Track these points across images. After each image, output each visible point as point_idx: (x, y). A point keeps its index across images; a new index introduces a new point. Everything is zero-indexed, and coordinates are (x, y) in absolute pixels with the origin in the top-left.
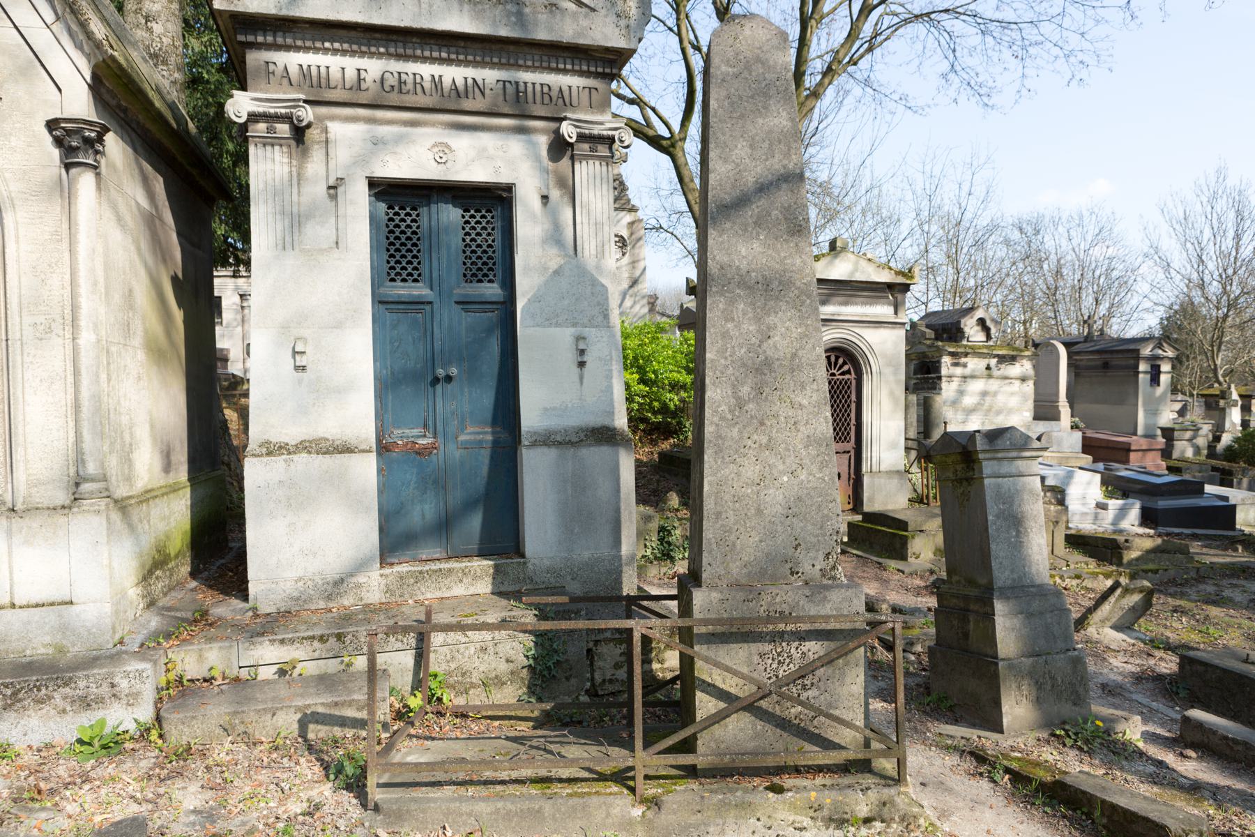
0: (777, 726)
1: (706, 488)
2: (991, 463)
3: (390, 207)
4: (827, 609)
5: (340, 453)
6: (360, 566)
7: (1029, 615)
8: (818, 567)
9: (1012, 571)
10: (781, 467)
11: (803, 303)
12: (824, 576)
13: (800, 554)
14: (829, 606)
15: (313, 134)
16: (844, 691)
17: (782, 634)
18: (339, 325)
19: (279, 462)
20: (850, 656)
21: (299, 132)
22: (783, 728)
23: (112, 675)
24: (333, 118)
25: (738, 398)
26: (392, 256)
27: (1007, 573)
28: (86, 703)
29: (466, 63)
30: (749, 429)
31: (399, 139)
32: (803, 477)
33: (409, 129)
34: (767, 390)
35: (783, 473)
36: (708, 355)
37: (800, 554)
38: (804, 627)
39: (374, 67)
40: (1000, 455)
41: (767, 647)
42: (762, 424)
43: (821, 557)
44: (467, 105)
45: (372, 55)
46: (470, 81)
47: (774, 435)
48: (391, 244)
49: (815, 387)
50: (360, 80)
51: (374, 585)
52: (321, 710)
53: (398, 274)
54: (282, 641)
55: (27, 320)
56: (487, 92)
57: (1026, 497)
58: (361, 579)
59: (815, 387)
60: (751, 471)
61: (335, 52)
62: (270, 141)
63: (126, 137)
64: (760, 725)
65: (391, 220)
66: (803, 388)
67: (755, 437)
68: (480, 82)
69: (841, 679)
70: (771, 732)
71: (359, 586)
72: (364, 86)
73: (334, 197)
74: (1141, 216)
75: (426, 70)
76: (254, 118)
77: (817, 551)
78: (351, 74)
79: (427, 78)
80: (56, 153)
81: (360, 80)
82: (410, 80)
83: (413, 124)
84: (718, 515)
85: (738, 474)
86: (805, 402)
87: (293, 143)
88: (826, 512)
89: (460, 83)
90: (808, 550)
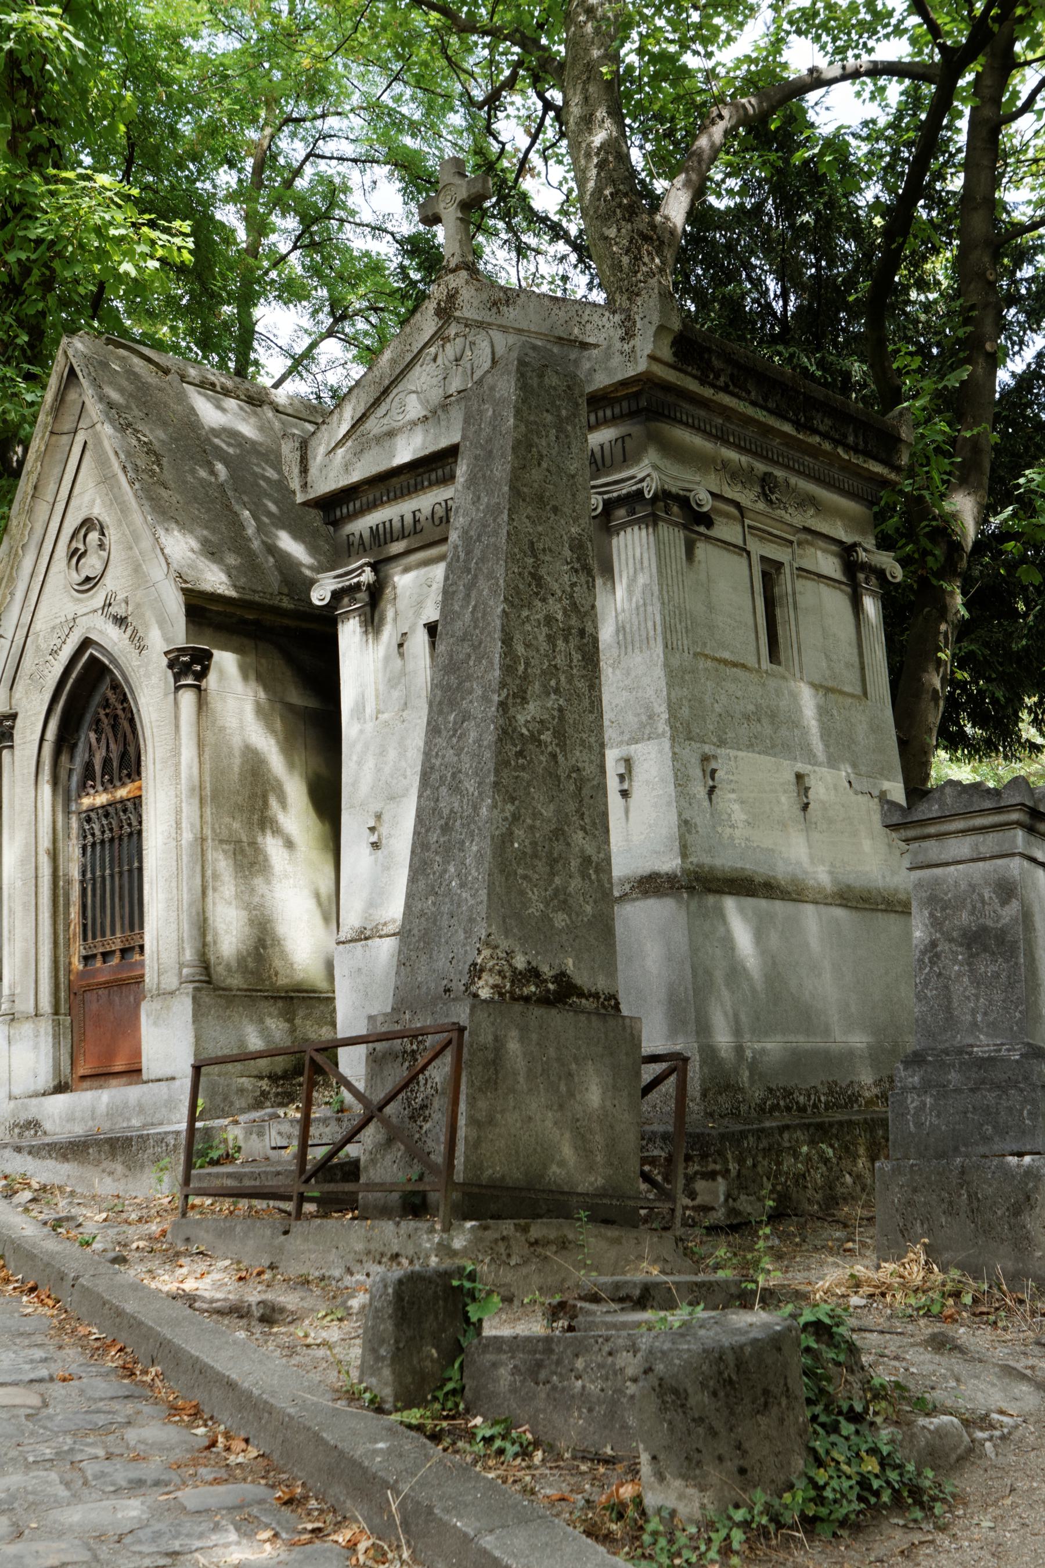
40: (932, 830)
73: (401, 655)
78: (409, 519)
81: (416, 521)
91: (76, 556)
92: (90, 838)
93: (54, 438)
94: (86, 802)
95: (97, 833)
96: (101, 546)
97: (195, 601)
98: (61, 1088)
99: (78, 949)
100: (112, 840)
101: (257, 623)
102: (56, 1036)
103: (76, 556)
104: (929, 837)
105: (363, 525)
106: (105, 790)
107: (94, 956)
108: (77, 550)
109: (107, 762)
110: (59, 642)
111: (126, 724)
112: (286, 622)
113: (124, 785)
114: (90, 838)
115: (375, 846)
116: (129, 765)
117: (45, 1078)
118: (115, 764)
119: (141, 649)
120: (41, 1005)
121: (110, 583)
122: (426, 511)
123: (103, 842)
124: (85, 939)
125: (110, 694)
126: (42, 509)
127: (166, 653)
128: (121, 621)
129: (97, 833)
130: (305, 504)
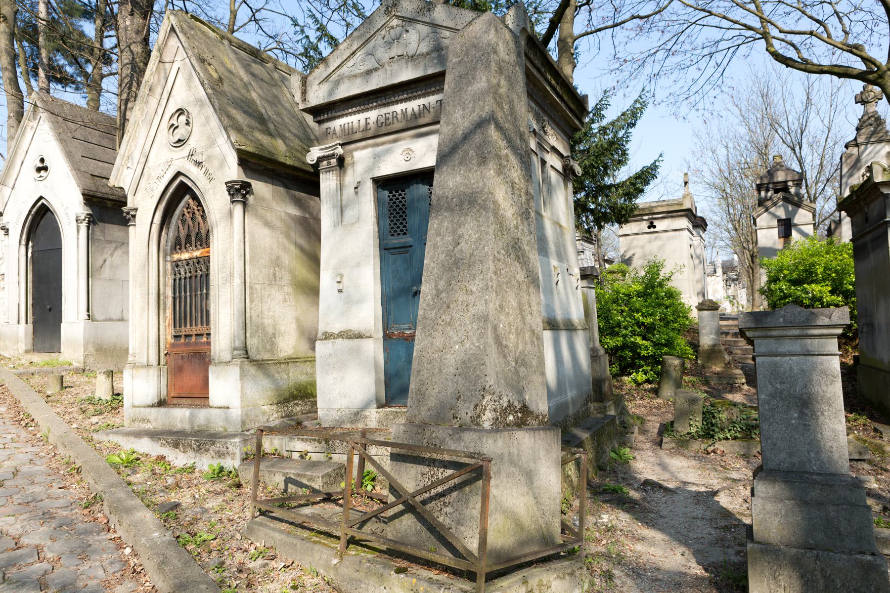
0: (428, 529)
1: (415, 354)
2: (766, 341)
3: (391, 192)
4: (460, 447)
5: (357, 338)
6: (366, 407)
7: (803, 503)
8: (469, 415)
9: (791, 455)
10: (455, 339)
11: (481, 214)
12: (472, 422)
13: (460, 404)
14: (462, 444)
15: (348, 160)
16: (467, 512)
17: (434, 460)
18: (358, 265)
19: (330, 342)
20: (473, 486)
21: (341, 161)
22: (431, 533)
23: (226, 443)
24: (356, 149)
25: (437, 290)
26: (392, 221)
27: (782, 456)
28: (220, 455)
29: (419, 97)
30: (441, 311)
31: (388, 151)
32: (467, 346)
33: (392, 145)
34: (453, 282)
35: (456, 343)
36: (425, 261)
37: (460, 404)
38: (447, 458)
39: (373, 115)
40: (774, 333)
41: (426, 469)
42: (448, 307)
43: (472, 407)
44: (422, 121)
45: (371, 109)
46: (422, 107)
47: (454, 314)
48: (391, 214)
49: (481, 277)
50: (367, 124)
51: (373, 417)
52: (292, 476)
53: (395, 231)
54: (302, 440)
55: (220, 276)
56: (431, 110)
57: (815, 378)
58: (367, 413)
59: (481, 277)
60: (439, 341)
61: (355, 113)
62: (329, 170)
63: (268, 180)
64: (419, 526)
65: (391, 200)
66: (474, 278)
67: (444, 317)
68: (427, 106)
69: (467, 502)
70: (425, 534)
71: (366, 417)
72: (369, 127)
73: (357, 193)
74: (42, 160)
75: (398, 108)
76: (320, 160)
77: (471, 402)
78: (363, 123)
79: (399, 112)
80: (229, 197)
81: (367, 124)
82: (390, 116)
83: (395, 141)
84: (419, 372)
85: (432, 344)
86: (474, 289)
87: (338, 168)
88: (478, 373)
89: (416, 109)
90: (464, 401)
91: (173, 128)
92: (178, 276)
93: (161, 64)
94: (176, 257)
95: (182, 273)
96: (188, 124)
97: (243, 157)
98: (161, 403)
99: (171, 331)
100: (190, 277)
101: (273, 170)
102: (159, 376)
103: (173, 128)
104: (772, 337)
105: (337, 124)
106: (187, 251)
107: (180, 336)
108: (173, 125)
109: (188, 236)
110: (162, 173)
111: (200, 218)
112: (287, 171)
113: (198, 249)
114: (178, 276)
115: (340, 291)
116: (203, 240)
117: (152, 398)
118: (193, 238)
119: (211, 180)
120: (150, 360)
121: (192, 143)
122: (409, 111)
123: (185, 278)
124: (175, 327)
125: (191, 201)
126: (153, 102)
127: (226, 183)
128: (199, 164)
129: (182, 273)
130: (303, 110)
